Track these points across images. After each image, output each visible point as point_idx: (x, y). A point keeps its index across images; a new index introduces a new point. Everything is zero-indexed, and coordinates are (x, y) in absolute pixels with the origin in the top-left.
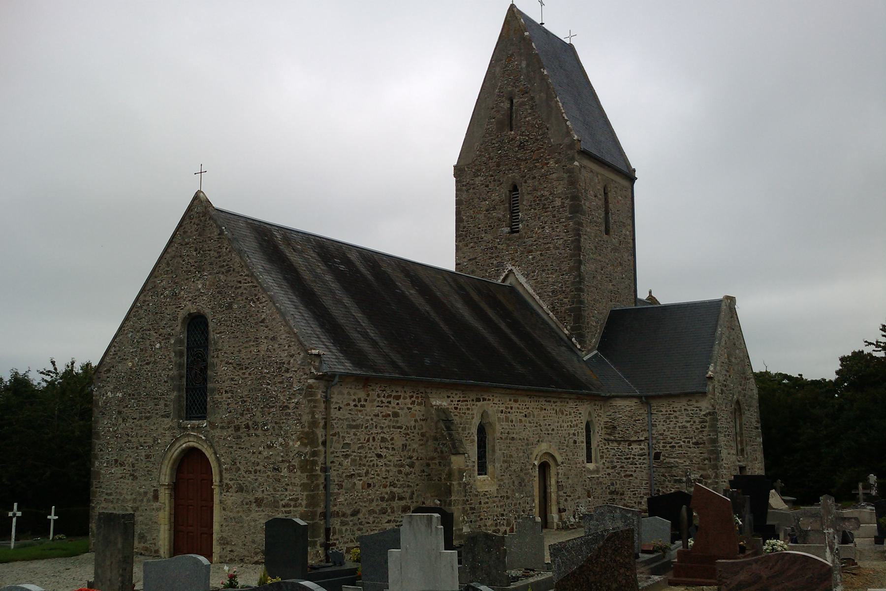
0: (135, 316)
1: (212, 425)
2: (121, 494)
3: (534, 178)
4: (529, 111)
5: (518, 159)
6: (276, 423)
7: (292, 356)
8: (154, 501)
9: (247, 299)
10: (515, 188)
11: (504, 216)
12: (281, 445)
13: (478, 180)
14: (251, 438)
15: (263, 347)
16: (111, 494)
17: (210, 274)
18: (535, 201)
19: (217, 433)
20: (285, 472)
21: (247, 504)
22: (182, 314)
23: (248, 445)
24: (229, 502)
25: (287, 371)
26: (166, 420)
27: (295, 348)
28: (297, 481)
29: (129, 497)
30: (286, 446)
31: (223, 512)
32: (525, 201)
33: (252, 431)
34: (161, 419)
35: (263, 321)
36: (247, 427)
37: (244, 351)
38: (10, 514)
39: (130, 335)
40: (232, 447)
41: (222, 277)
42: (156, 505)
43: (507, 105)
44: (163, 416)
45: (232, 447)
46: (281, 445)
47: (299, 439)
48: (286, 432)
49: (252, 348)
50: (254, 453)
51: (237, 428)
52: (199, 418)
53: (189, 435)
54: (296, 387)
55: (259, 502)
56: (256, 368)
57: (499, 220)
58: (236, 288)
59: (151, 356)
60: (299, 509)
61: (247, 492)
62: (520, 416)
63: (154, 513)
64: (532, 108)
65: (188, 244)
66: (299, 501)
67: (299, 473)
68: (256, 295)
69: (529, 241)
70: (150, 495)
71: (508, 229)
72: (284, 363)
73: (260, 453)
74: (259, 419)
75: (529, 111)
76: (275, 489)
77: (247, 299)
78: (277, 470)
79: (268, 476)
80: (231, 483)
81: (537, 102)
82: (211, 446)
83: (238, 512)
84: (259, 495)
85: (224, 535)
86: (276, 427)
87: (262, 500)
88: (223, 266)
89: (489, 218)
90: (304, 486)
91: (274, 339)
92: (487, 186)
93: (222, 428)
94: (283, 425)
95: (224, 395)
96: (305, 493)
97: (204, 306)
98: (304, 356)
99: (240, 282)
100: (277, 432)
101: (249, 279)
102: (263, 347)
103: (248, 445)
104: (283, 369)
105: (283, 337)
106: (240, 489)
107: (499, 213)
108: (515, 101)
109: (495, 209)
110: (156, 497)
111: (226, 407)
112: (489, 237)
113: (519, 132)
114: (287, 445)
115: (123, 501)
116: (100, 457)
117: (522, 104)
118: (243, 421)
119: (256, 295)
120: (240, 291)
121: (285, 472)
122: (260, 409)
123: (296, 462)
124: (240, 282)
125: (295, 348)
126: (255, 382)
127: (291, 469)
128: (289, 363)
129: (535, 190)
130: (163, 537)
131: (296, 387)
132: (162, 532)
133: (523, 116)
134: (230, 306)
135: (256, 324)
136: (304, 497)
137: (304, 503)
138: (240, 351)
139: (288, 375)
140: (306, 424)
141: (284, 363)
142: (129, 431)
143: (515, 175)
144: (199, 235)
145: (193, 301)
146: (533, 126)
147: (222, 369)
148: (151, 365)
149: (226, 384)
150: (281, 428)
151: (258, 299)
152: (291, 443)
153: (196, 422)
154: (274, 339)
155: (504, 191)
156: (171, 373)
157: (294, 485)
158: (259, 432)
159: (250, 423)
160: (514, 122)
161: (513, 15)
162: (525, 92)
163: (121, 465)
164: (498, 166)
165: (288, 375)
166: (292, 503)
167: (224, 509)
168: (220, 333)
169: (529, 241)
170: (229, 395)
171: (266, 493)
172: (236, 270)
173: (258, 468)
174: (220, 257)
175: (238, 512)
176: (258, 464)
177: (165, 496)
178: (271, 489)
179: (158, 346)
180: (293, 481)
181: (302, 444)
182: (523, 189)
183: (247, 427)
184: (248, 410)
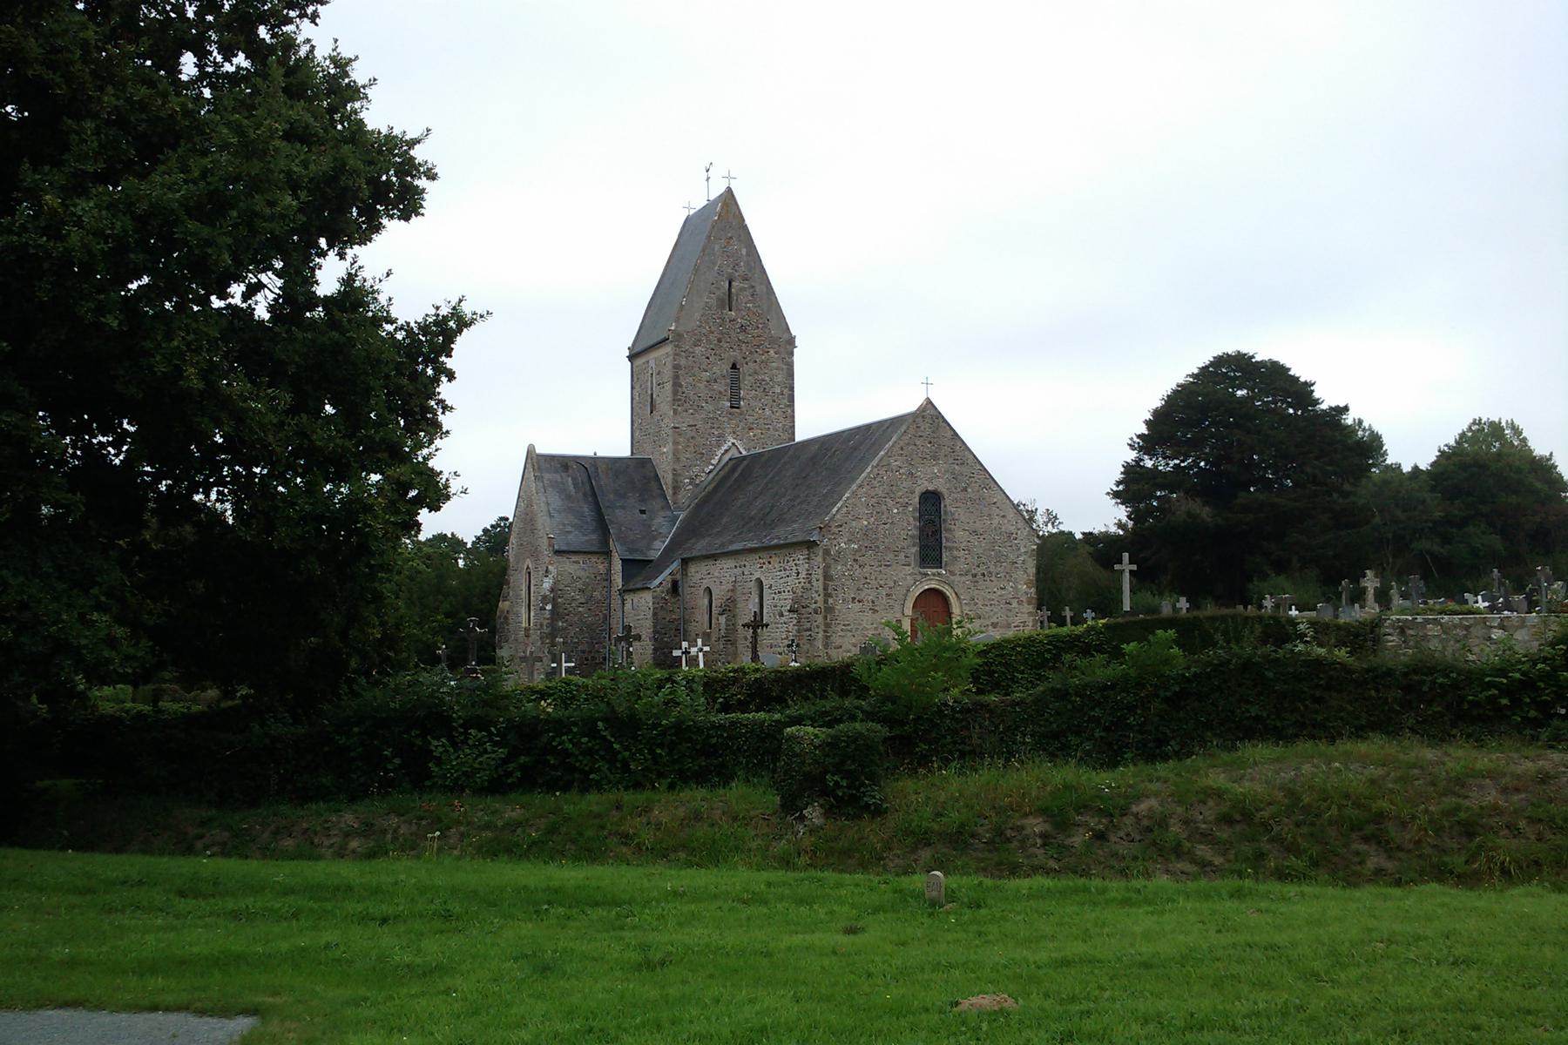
1: (952, 573)
10: (734, 367)
15: (995, 522)
19: (957, 578)
20: (1015, 604)
30: (1015, 588)
32: (747, 381)
38: (676, 653)
55: (994, 625)
69: (751, 419)
74: (992, 569)
90: (1030, 614)
97: (939, 485)
102: (995, 522)
112: (710, 407)
118: (979, 571)
121: (1015, 604)
130: (1314, 614)
134: (965, 489)
143: (735, 354)
145: (930, 480)
155: (726, 367)
161: (728, 198)
169: (751, 419)
182: (743, 369)
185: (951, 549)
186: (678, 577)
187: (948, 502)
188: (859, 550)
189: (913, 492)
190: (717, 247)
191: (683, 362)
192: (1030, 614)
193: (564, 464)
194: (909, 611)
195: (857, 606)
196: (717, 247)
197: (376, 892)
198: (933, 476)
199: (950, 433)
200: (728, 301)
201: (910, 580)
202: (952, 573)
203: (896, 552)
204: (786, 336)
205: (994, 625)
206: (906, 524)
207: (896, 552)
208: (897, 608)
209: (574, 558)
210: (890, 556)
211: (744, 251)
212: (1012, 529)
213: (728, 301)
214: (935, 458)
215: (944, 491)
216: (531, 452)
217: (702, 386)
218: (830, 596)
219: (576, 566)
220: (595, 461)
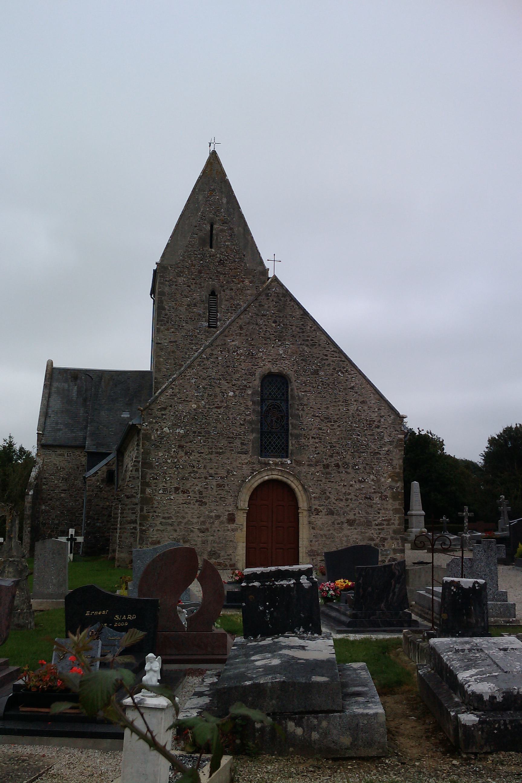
0: (199, 365)
1: (299, 463)
2: (184, 518)
3: (232, 289)
4: (229, 238)
5: (217, 271)
6: (367, 464)
7: (381, 417)
8: (229, 523)
9: (334, 369)
10: (213, 293)
11: (204, 313)
12: (373, 480)
13: (180, 280)
14: (341, 475)
15: (353, 408)
16: (169, 518)
17: (293, 344)
18: (231, 307)
19: (304, 469)
21: (338, 524)
22: (259, 372)
23: (338, 479)
24: (319, 523)
25: (378, 427)
26: (243, 456)
27: (386, 411)
28: (389, 507)
29: (195, 521)
31: (312, 530)
33: (341, 469)
34: (236, 455)
35: (352, 388)
36: (337, 466)
37: (331, 408)
39: (193, 381)
40: (321, 481)
41: (306, 348)
42: (233, 526)
43: (208, 228)
44: (239, 453)
45: (321, 481)
46: (373, 480)
47: (390, 477)
48: (378, 471)
49: (341, 407)
50: (344, 486)
51: (327, 466)
52: (282, 457)
53: (273, 470)
54: (386, 439)
55: (351, 523)
56: (346, 422)
57: (200, 315)
58: (322, 359)
59: (222, 402)
60: (392, 526)
61: (339, 515)
62: (199, 471)
63: (228, 533)
64: (231, 236)
65: (263, 315)
66: (392, 521)
67: (391, 501)
68: (344, 368)
70: (224, 518)
71: (206, 324)
72: (374, 421)
73: (351, 486)
75: (229, 238)
76: (367, 513)
77: (334, 369)
78: (370, 498)
79: (360, 503)
80: (321, 508)
81: (236, 232)
82: (299, 480)
83: (329, 530)
84: (351, 517)
85: (314, 548)
86: (367, 467)
87: (355, 520)
88: (308, 340)
89: (190, 312)
90: (396, 511)
91: (363, 402)
92: (189, 286)
93: (309, 465)
94: (374, 466)
95: (311, 441)
96: (398, 515)
97: (285, 367)
98: (394, 419)
99: (326, 355)
100: (368, 471)
101: (337, 355)
102: (353, 408)
103: (338, 479)
104: (374, 425)
105: (373, 402)
106: (331, 513)
107: (200, 310)
108: (215, 226)
109: (195, 305)
110: (232, 519)
111: (314, 449)
112: (191, 327)
113: (219, 252)
114: (379, 480)
115: (186, 524)
116: (153, 485)
117: (222, 231)
119: (344, 368)
120: (327, 363)
121: (377, 500)
122: (349, 453)
123: (389, 493)
124: (326, 355)
125: (386, 411)
126: (344, 432)
127: (383, 498)
128: (379, 422)
129: (232, 298)
131: (386, 439)
132: (239, 548)
133: (223, 240)
134: (316, 372)
135: (345, 389)
136: (397, 518)
137: (397, 522)
138: (328, 408)
139: (379, 430)
140: (397, 466)
141: (374, 421)
142: (195, 463)
144: (279, 311)
145: (274, 362)
146: (232, 250)
147: (308, 420)
148: (222, 410)
149: (313, 432)
150: (373, 468)
151: (346, 371)
152: (383, 480)
153: (278, 460)
154: (363, 402)
155: (205, 294)
156: (248, 418)
157: (386, 509)
158: (350, 470)
159: (340, 463)
160: (214, 242)
162: (224, 222)
163: (184, 492)
164: (200, 272)
165: (379, 430)
166: (385, 523)
167: (313, 528)
168: (305, 391)
170: (317, 440)
171: (357, 515)
172: (322, 345)
173: (349, 497)
174: (303, 332)
175: (329, 530)
176: (349, 494)
177: (241, 519)
178: (364, 513)
179: (231, 394)
180: (386, 507)
181: (393, 480)
182: (221, 295)
183: (337, 466)
184: (337, 453)
185: (297, 437)
186: (114, 467)
187: (294, 385)
188: (186, 435)
189: (253, 374)
190: (201, 198)
191: (167, 289)
192: (396, 511)
193: (74, 375)
194: (244, 503)
195: (181, 498)
196: (201, 198)
197: (423, 611)
198: (276, 357)
199: (298, 313)
200: (210, 240)
201: (246, 470)
202: (299, 463)
203: (231, 439)
204: (260, 268)
205: (351, 523)
206: (242, 408)
207: (231, 439)
208: (230, 500)
209: (59, 451)
210: (223, 442)
211: (225, 201)
212: (374, 416)
213: (210, 240)
214: (281, 338)
215: (291, 373)
216: (50, 364)
217: (183, 309)
218: (148, 485)
219: (61, 458)
220: (101, 374)
